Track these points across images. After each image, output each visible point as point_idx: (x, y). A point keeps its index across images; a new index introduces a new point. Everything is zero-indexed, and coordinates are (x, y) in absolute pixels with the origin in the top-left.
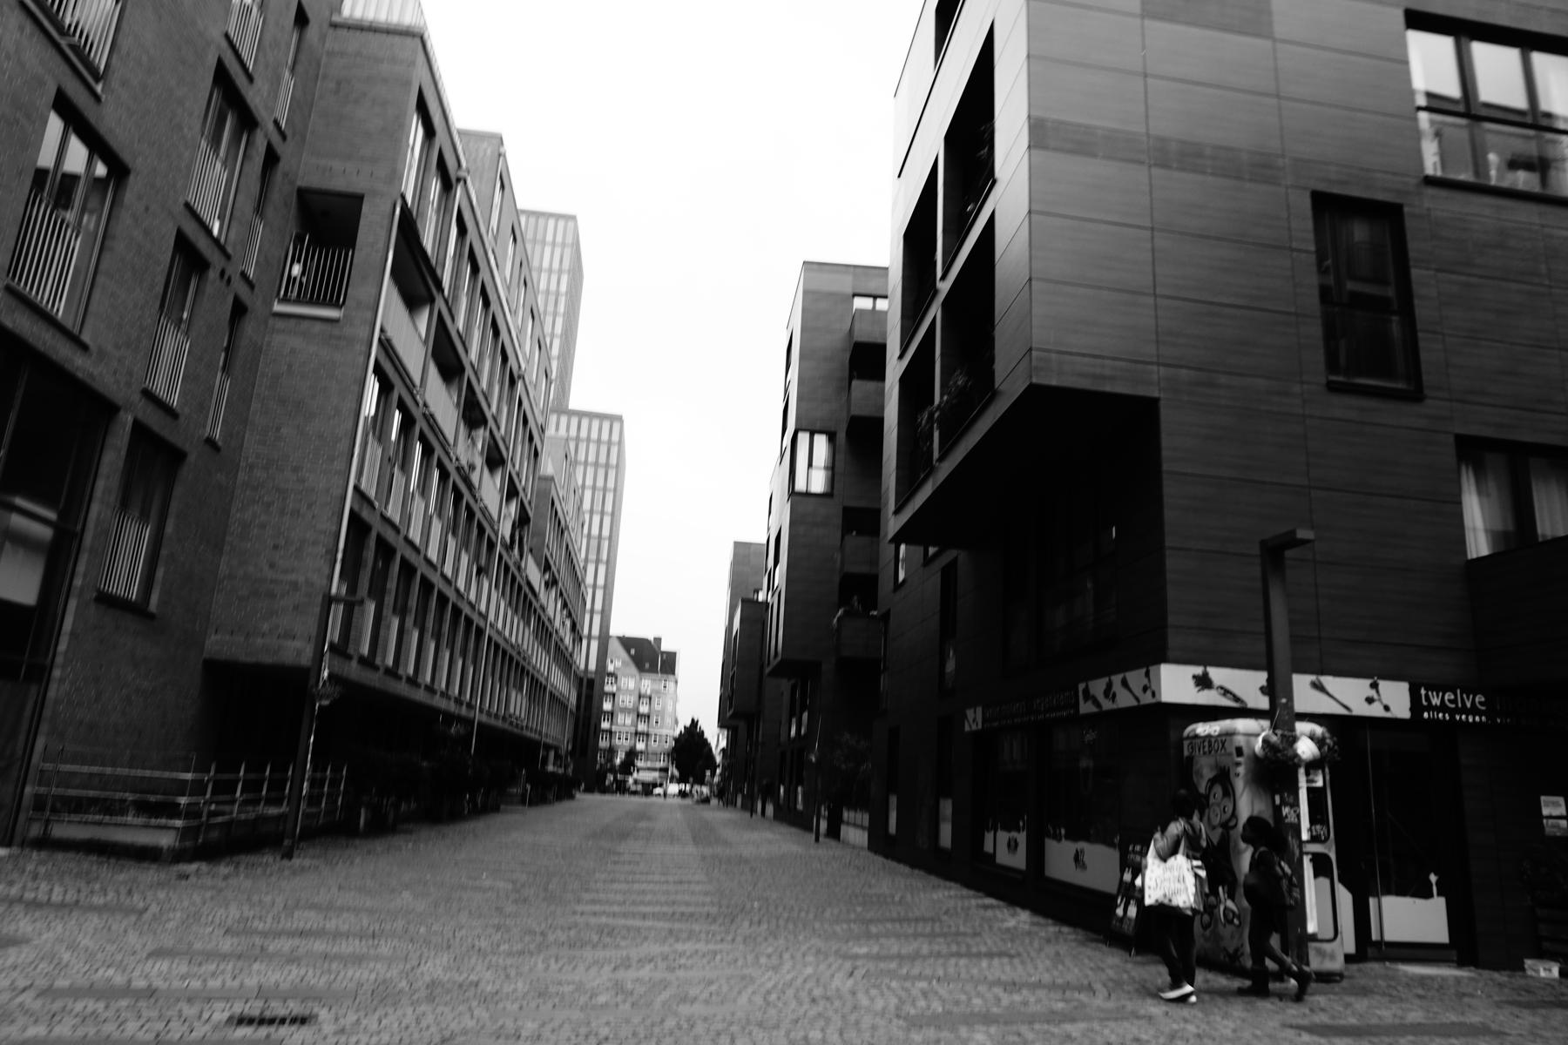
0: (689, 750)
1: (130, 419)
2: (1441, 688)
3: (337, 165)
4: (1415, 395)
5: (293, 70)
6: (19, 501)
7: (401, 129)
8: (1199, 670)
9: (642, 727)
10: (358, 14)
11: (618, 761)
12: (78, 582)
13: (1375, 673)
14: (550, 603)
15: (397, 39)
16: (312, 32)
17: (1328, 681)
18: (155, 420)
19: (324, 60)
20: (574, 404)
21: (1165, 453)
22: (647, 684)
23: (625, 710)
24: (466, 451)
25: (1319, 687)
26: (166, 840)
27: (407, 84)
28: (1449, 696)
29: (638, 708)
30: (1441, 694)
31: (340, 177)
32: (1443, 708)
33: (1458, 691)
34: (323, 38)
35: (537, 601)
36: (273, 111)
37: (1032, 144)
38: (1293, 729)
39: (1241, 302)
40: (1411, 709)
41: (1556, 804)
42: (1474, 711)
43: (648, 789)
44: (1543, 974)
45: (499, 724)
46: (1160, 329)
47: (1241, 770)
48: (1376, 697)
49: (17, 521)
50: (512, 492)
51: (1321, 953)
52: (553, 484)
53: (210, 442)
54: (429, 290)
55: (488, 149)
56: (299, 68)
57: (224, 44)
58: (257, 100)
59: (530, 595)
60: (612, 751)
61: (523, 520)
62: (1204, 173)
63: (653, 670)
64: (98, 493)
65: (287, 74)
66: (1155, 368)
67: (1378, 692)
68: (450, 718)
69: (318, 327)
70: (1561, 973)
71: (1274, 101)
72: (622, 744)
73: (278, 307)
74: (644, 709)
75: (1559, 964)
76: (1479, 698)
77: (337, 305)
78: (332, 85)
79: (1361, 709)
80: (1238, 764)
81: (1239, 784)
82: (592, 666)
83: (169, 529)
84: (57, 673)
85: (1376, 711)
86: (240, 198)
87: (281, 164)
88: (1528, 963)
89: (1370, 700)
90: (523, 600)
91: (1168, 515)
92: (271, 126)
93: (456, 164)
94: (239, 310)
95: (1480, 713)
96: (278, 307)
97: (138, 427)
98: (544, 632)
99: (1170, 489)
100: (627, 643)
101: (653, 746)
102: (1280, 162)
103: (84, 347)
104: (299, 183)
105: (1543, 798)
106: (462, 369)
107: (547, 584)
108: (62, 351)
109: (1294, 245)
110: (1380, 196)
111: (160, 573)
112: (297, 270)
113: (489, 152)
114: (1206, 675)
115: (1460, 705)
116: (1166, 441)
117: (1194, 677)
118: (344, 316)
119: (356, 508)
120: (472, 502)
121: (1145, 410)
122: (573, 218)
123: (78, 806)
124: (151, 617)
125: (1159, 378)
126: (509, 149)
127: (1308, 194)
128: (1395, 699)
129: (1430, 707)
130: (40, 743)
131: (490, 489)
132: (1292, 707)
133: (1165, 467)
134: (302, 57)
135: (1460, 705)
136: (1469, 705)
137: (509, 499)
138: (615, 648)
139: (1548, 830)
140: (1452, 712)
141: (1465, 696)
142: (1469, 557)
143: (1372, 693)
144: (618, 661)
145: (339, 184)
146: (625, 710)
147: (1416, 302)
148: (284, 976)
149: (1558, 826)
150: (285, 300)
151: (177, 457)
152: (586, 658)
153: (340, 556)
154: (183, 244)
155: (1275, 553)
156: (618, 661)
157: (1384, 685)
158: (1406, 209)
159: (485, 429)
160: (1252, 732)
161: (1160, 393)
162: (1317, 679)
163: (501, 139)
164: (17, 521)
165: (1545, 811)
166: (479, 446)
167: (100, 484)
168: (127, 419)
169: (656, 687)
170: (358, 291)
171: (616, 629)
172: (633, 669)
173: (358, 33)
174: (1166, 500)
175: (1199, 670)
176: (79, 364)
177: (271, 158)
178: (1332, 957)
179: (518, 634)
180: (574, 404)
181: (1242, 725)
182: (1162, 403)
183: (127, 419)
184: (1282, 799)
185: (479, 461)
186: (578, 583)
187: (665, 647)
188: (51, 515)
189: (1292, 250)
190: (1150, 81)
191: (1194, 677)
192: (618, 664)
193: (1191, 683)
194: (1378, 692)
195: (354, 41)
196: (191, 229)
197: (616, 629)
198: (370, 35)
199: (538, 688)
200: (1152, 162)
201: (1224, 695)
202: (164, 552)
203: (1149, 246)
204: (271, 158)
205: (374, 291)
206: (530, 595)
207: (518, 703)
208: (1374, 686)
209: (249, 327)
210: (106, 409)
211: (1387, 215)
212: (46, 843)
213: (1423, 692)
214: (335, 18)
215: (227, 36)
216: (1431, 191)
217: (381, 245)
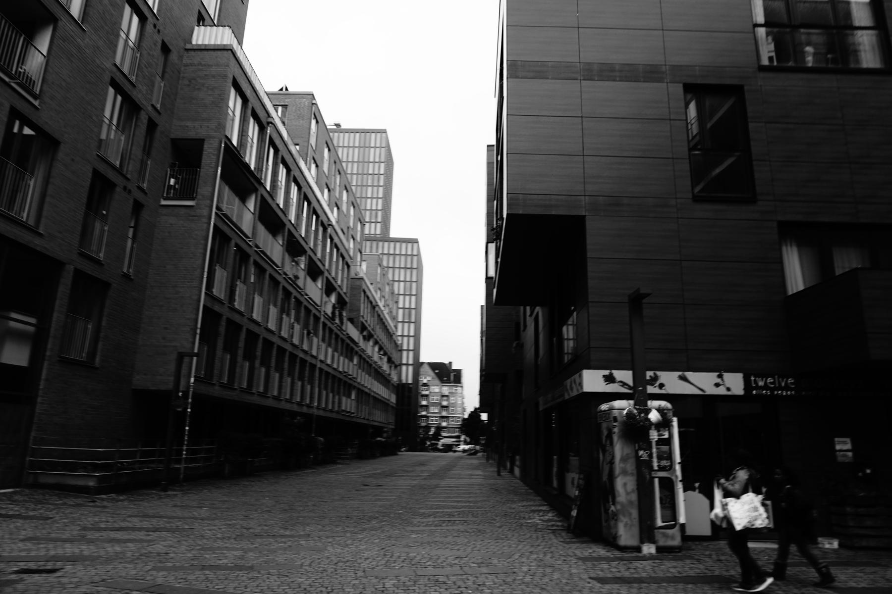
0: (471, 425)
1: (72, 267)
2: (764, 376)
3: (189, 124)
4: (752, 200)
5: (163, 77)
6: (14, 315)
7: (225, 100)
8: (607, 372)
9: (444, 413)
10: (200, 43)
11: (431, 433)
12: (48, 353)
13: (720, 369)
14: (371, 350)
15: (219, 53)
16: (173, 57)
17: (690, 375)
18: (88, 268)
19: (183, 69)
20: (393, 234)
21: (589, 247)
22: (446, 390)
23: (434, 404)
24: (291, 269)
25: (683, 378)
26: (91, 483)
27: (225, 76)
28: (770, 380)
29: (441, 404)
30: (764, 379)
31: (193, 129)
32: (766, 387)
33: (776, 377)
34: (181, 57)
35: (358, 347)
36: (151, 100)
37: (508, 77)
38: (646, 405)
39: (637, 154)
40: (744, 389)
41: (845, 443)
42: (786, 388)
43: (448, 448)
44: (827, 546)
45: (334, 416)
46: (586, 175)
47: (616, 430)
48: (721, 383)
49: (13, 324)
50: (329, 288)
51: (666, 536)
52: (363, 283)
53: (126, 276)
54: (255, 186)
55: (306, 102)
56: (167, 76)
57: (115, 69)
58: (140, 96)
59: (352, 345)
60: (428, 428)
61: (341, 303)
62: (614, 80)
63: (448, 381)
64: (57, 308)
65: (158, 79)
66: (583, 197)
67: (722, 380)
68: (293, 414)
69: (183, 211)
70: (840, 545)
71: (661, 32)
72: (434, 422)
73: (163, 202)
74: (445, 403)
75: (838, 540)
76: (790, 381)
77: (193, 199)
78: (187, 82)
79: (711, 390)
80: (615, 427)
81: (615, 438)
82: (410, 381)
83: (104, 323)
84: (39, 400)
85: (721, 391)
86: (134, 148)
87: (159, 128)
88: (820, 539)
89: (717, 385)
90: (349, 349)
91: (591, 283)
92: (150, 108)
93: (266, 115)
94: (138, 207)
95: (791, 390)
96: (163, 202)
97: (78, 273)
98: (367, 365)
99: (591, 267)
100: (434, 366)
101: (452, 423)
102: (664, 68)
103: (40, 235)
104: (173, 136)
105: (836, 439)
106: (284, 225)
107: (364, 337)
108: (25, 238)
109: (672, 117)
110: (728, 81)
111: (100, 345)
112: (172, 181)
113: (307, 103)
114: (611, 374)
115: (777, 385)
116: (589, 240)
117: (604, 376)
118: (197, 204)
119: (209, 305)
120: (299, 296)
121: (580, 221)
122: (384, 132)
123: (54, 466)
124: (96, 368)
125: (585, 203)
126: (319, 101)
127: (681, 85)
128: (735, 383)
129: (758, 388)
130: (33, 434)
131: (314, 290)
132: (646, 391)
133: (589, 255)
134: (168, 70)
135: (777, 385)
136: (783, 384)
137: (328, 294)
138: (426, 369)
139: (840, 459)
140: (772, 390)
141: (780, 379)
142: (790, 293)
143: (719, 381)
144: (427, 377)
145: (192, 134)
146: (434, 404)
147: (752, 143)
148: (41, 550)
149: (845, 456)
150: (166, 199)
151: (107, 285)
152: (407, 375)
153: (198, 331)
154: (96, 173)
155: (636, 301)
156: (427, 377)
157: (726, 376)
158: (746, 88)
159: (306, 255)
160: (623, 406)
161: (585, 213)
162: (655, 374)
163: (313, 95)
164: (13, 324)
165: (838, 447)
166: (303, 266)
167: (58, 303)
168: (70, 268)
169: (451, 391)
170: (203, 190)
171: (425, 357)
172: (437, 381)
173: (199, 53)
174: (590, 274)
175: (607, 372)
176: (37, 243)
177: (152, 126)
178: (673, 538)
179: (344, 365)
180: (393, 234)
181: (618, 404)
182: (587, 218)
183: (70, 268)
184: (639, 446)
185: (302, 274)
186: (390, 335)
187: (454, 367)
188: (33, 321)
189: (670, 120)
190: (580, 29)
191: (604, 376)
192: (429, 378)
193: (602, 380)
194: (722, 380)
195: (197, 58)
196: (102, 168)
197: (425, 357)
198: (206, 52)
199: (364, 395)
200: (582, 78)
201: (622, 386)
202: (102, 335)
203: (580, 127)
204: (152, 126)
205: (210, 189)
206: (352, 345)
207: (348, 404)
208: (720, 376)
209: (145, 215)
210: (58, 265)
211: (735, 91)
212: (36, 486)
213: (753, 378)
214: (188, 46)
215: (115, 65)
216: (762, 75)
217: (213, 165)
